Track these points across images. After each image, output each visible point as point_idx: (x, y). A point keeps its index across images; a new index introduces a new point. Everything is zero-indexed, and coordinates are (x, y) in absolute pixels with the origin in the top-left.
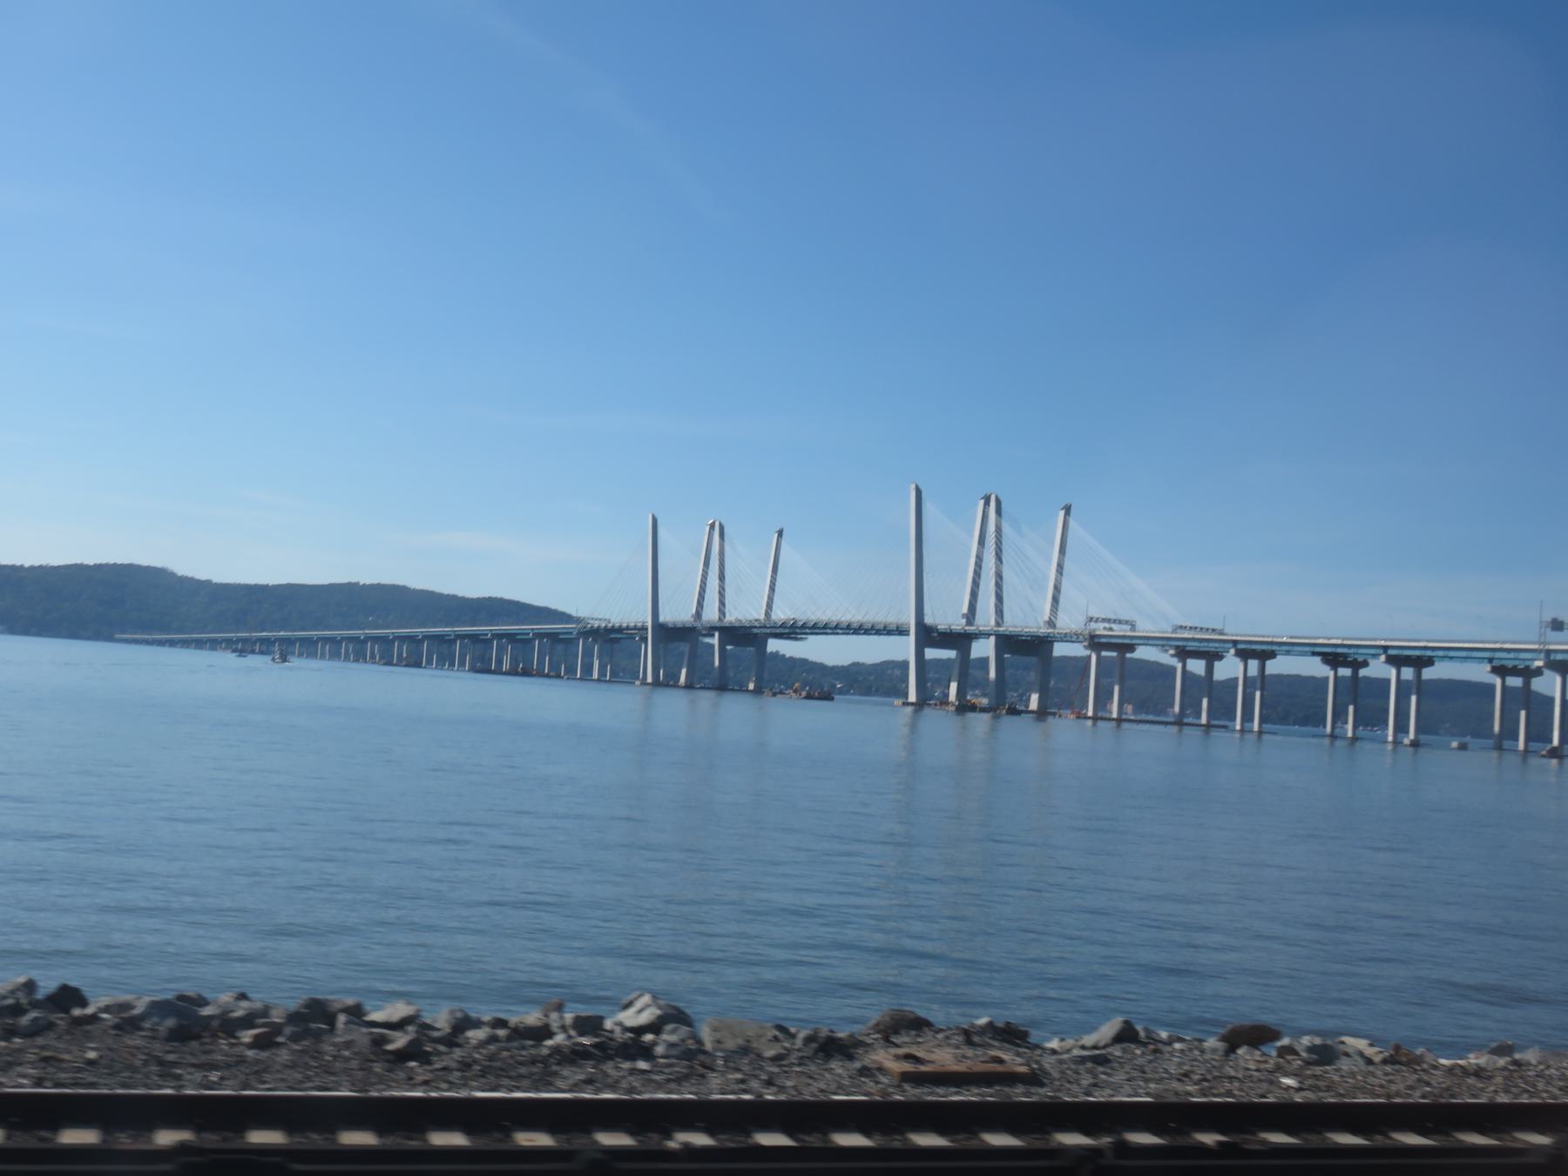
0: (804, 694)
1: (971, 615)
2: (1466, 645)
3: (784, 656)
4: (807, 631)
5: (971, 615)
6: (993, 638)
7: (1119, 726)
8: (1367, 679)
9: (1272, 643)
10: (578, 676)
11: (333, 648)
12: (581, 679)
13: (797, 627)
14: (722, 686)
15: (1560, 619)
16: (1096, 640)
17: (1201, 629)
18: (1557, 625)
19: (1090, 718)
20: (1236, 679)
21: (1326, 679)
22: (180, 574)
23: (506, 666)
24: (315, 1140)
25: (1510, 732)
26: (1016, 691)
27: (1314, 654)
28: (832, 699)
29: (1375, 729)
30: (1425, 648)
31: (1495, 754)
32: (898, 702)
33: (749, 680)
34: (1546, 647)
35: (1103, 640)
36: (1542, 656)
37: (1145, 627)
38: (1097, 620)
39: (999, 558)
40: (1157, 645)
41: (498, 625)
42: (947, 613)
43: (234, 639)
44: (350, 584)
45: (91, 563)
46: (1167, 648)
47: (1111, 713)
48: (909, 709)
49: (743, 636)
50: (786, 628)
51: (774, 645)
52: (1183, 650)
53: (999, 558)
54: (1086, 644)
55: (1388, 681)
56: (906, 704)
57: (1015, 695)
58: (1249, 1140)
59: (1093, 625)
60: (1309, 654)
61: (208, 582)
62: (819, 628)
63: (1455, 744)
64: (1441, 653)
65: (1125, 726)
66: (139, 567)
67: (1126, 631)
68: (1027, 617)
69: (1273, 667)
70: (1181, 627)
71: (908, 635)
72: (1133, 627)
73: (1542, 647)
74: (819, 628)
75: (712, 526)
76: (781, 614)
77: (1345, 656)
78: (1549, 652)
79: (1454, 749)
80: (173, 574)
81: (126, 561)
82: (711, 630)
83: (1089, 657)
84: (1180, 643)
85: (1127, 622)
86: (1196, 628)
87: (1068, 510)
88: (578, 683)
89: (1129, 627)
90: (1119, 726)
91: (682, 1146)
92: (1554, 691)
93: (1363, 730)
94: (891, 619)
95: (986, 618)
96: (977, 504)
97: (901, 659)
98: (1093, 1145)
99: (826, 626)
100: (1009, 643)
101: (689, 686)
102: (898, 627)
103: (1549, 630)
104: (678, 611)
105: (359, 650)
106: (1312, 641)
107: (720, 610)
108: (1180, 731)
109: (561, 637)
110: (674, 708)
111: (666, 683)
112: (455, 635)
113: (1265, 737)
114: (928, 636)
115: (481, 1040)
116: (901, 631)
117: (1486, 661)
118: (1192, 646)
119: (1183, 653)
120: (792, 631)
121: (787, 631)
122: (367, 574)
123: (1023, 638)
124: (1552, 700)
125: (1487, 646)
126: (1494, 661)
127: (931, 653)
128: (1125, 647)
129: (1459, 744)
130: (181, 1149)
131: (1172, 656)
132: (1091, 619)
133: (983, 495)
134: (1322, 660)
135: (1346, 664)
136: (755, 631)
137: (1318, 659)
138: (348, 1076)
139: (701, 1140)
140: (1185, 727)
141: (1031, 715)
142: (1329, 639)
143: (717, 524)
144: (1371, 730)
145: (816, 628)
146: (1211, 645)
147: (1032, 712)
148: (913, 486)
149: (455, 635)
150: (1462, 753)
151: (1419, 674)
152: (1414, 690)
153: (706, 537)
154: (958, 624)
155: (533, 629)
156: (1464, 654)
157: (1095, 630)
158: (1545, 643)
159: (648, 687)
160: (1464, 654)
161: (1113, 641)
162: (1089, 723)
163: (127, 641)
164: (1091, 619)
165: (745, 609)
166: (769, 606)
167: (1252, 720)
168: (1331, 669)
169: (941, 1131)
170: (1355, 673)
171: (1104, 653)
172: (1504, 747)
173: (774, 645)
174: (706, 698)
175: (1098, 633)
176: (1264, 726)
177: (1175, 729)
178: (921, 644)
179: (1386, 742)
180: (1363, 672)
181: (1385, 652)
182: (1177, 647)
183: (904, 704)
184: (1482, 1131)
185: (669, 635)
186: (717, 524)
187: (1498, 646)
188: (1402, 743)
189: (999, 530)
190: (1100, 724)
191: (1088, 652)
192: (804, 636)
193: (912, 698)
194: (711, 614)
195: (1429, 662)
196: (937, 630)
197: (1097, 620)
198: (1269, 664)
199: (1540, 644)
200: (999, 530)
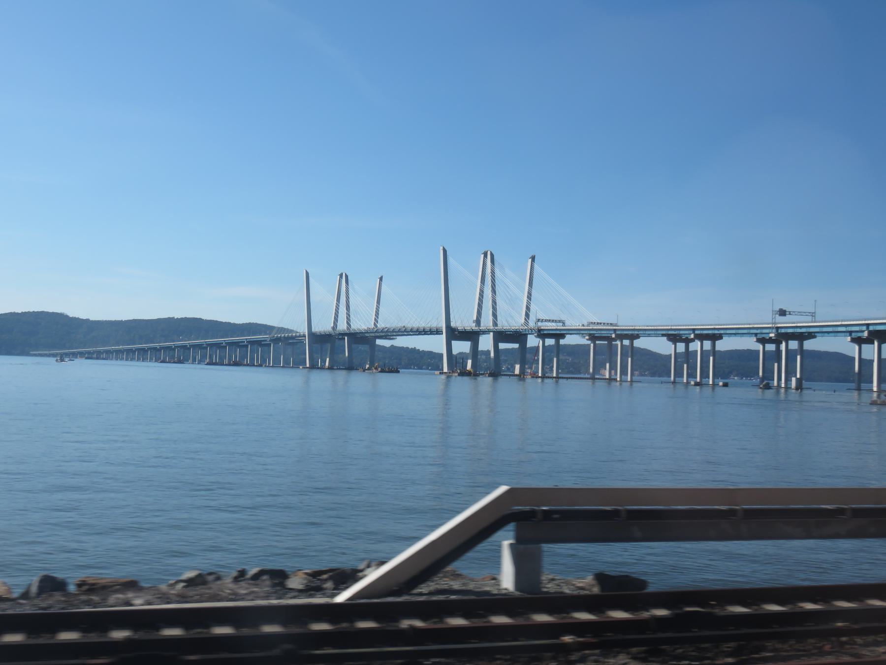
0: (379, 369)
1: (478, 322)
2: (735, 326)
3: (419, 350)
4: (394, 334)
5: (478, 322)
6: (492, 333)
7: (609, 384)
8: (565, 346)
9: (634, 330)
10: (308, 365)
11: (118, 355)
12: (283, 367)
13: (390, 332)
14: (350, 367)
15: (784, 309)
16: (542, 332)
17: (604, 324)
18: (782, 313)
19: (539, 377)
20: (671, 355)
21: (589, 345)
22: (71, 316)
23: (226, 361)
24: (197, 632)
25: (679, 374)
26: (549, 365)
27: (663, 335)
28: (398, 372)
29: (752, 379)
30: (714, 329)
31: (856, 393)
32: (437, 372)
33: (365, 363)
34: (776, 326)
35: (545, 332)
36: (774, 331)
37: (572, 323)
38: (542, 321)
39: (494, 291)
40: (579, 334)
41: (228, 338)
42: (463, 320)
43: (92, 352)
44: (169, 319)
45: (20, 312)
46: (584, 335)
47: (605, 376)
48: (443, 377)
49: (358, 338)
50: (379, 332)
51: (379, 342)
52: (593, 336)
53: (494, 291)
54: (536, 335)
55: (759, 351)
56: (442, 373)
57: (548, 367)
58: (94, 588)
59: (540, 324)
60: (661, 335)
61: (88, 320)
62: (402, 332)
63: (721, 384)
64: (642, 332)
65: (561, 381)
66: (48, 313)
67: (560, 326)
68: (512, 320)
69: (721, 346)
70: (592, 323)
71: (442, 334)
72: (564, 323)
73: (774, 325)
74: (402, 332)
75: (341, 276)
76: (381, 325)
77: (680, 335)
78: (778, 328)
79: (692, 385)
80: (67, 316)
81: (40, 310)
82: (343, 334)
83: (589, 345)
84: (591, 332)
85: (560, 321)
86: (601, 323)
87: (533, 258)
88: (270, 370)
89: (561, 324)
90: (609, 384)
91: (409, 627)
92: (855, 355)
93: (746, 379)
94: (434, 324)
95: (487, 322)
96: (528, 262)
97: (668, 354)
98: (631, 618)
99: (411, 330)
100: (501, 336)
101: (331, 368)
102: (430, 330)
103: (777, 316)
104: (322, 325)
105: (142, 354)
106: (655, 328)
107: (334, 323)
108: (674, 387)
109: (241, 344)
110: (322, 381)
111: (321, 367)
112: (206, 344)
113: (635, 384)
114: (454, 334)
115: (429, 581)
116: (438, 332)
117: (754, 335)
118: (597, 334)
119: (593, 338)
120: (388, 334)
121: (384, 334)
122: (178, 313)
123: (509, 333)
124: (854, 359)
125: (746, 326)
126: (758, 335)
127: (502, 346)
128: (558, 336)
129: (723, 383)
130: (127, 642)
131: (587, 339)
132: (539, 320)
133: (483, 252)
134: (667, 339)
135: (681, 340)
136: (367, 335)
137: (665, 338)
138: (64, 596)
139: (418, 624)
140: (596, 380)
141: (515, 377)
142: (635, 326)
143: (344, 275)
144: (750, 380)
145: (388, 332)
146: (603, 332)
147: (516, 375)
148: (442, 248)
149: (206, 344)
150: (725, 388)
151: (801, 345)
152: (712, 354)
153: (338, 282)
154: (470, 325)
155: (225, 340)
156: (733, 332)
157: (540, 327)
158: (775, 323)
159: (307, 369)
160: (733, 332)
161: (551, 332)
162: (540, 380)
163: (36, 355)
164: (539, 320)
165: (362, 323)
166: (376, 320)
167: (627, 375)
168: (673, 344)
169: (549, 612)
170: (557, 342)
171: (597, 342)
172: (862, 389)
173: (379, 342)
174: (341, 375)
175: (542, 328)
176: (677, 379)
177: (590, 382)
178: (497, 341)
179: (872, 390)
180: (562, 342)
181: (694, 332)
182: (590, 335)
183: (440, 373)
184: (848, 600)
185: (320, 340)
186: (344, 275)
187: (751, 326)
188: (718, 385)
189: (493, 272)
190: (546, 381)
191: (589, 342)
192: (395, 337)
193: (445, 370)
194: (342, 326)
195: (720, 337)
196: (458, 330)
197: (542, 321)
198: (718, 343)
199: (773, 324)
200: (493, 272)
